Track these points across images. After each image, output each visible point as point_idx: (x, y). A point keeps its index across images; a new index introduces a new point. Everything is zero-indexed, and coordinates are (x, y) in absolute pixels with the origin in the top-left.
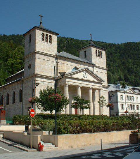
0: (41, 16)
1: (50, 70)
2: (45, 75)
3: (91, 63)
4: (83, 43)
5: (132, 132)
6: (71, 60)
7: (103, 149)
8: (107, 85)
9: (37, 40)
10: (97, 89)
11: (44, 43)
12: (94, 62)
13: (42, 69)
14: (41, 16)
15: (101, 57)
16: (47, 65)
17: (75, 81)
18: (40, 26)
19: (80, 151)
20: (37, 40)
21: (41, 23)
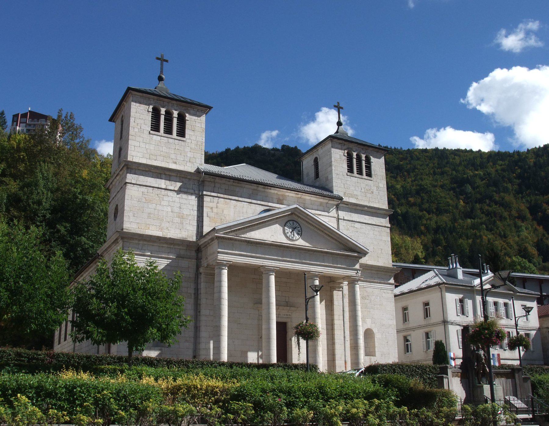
0: (162, 60)
1: (177, 220)
2: (159, 234)
3: (332, 194)
4: (411, 157)
5: (321, 301)
6: (443, 301)
7: (129, 186)
8: (390, 266)
9: (136, 130)
10: (345, 278)
11: (160, 138)
12: (338, 190)
13: (149, 217)
14: (162, 60)
15: (369, 174)
16: (164, 203)
17: (348, 320)
18: (337, 132)
19: (114, 206)
20: (136, 130)
21: (160, 79)
